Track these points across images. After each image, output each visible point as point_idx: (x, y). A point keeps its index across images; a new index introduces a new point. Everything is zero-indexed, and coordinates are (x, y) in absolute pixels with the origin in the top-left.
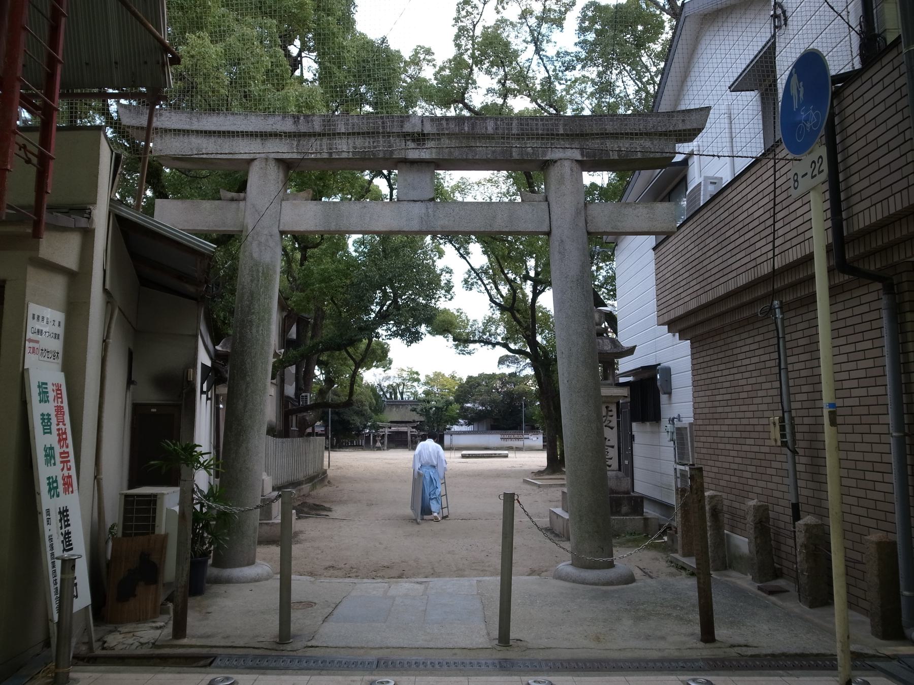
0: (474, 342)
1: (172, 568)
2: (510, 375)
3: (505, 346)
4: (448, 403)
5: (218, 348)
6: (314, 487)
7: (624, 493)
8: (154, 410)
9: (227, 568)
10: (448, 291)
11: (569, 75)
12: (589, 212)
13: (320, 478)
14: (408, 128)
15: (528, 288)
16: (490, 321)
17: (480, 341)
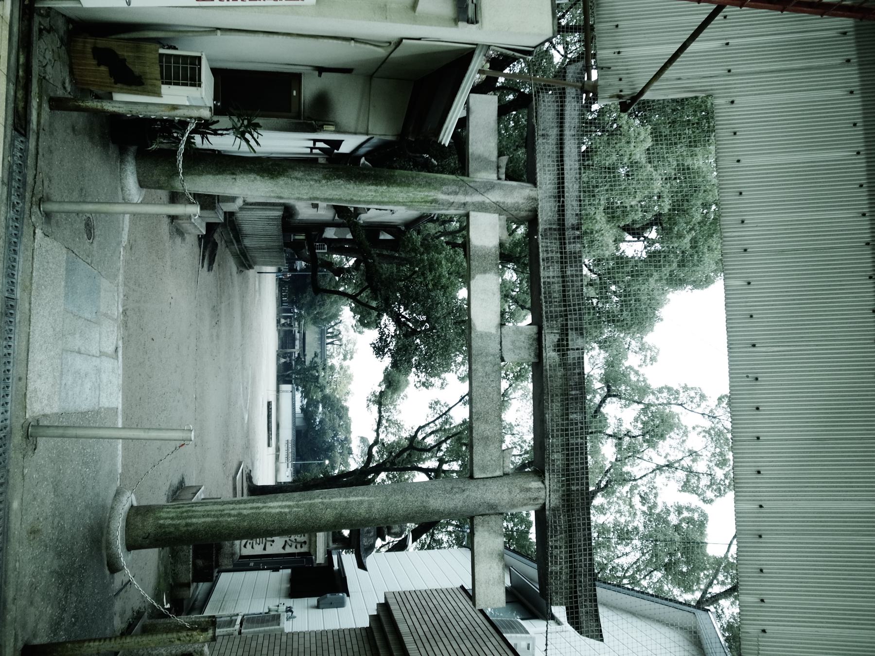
0: (380, 412)
1: (125, 101)
2: (350, 449)
3: (376, 442)
4: (322, 388)
5: (363, 160)
6: (234, 255)
8: (295, 93)
9: (136, 161)
10: (424, 384)
11: (636, 500)
13: (245, 262)
14: (572, 335)
15: (432, 464)
16: (400, 427)
17: (380, 417)
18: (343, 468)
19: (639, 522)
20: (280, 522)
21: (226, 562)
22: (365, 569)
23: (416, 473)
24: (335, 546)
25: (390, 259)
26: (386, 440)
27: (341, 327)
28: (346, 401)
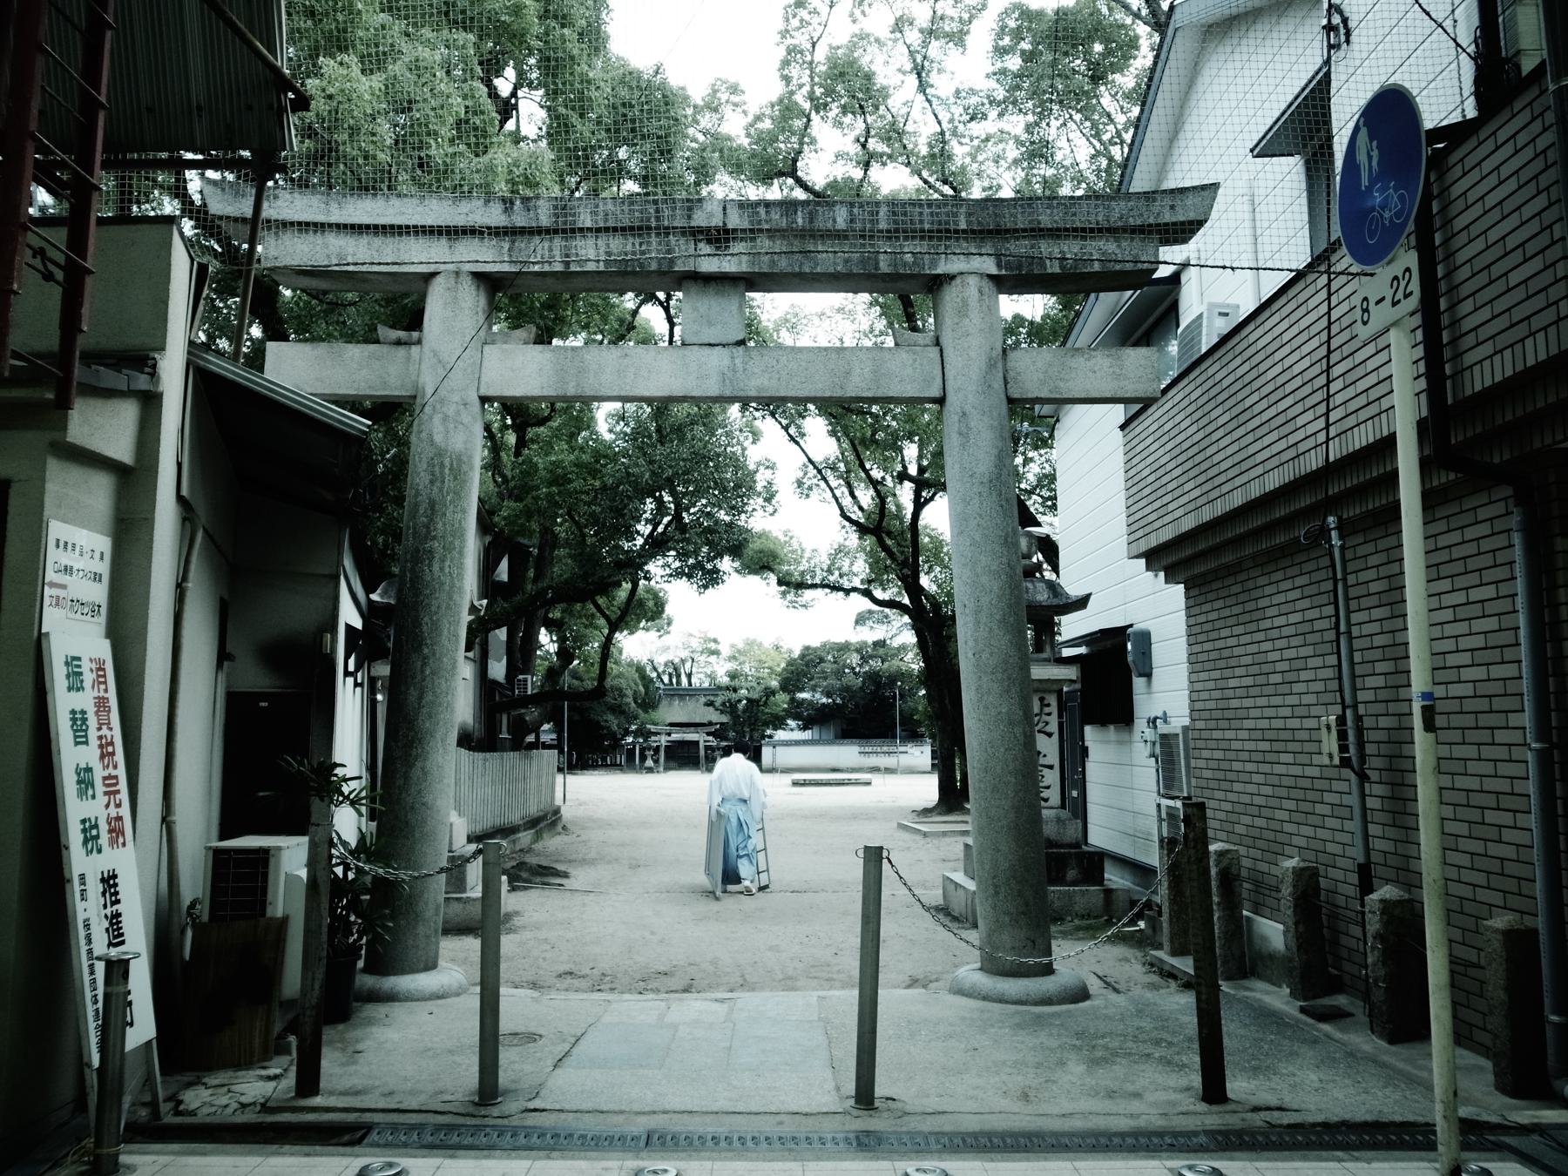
0: (814, 586)
2: (877, 644)
3: (867, 593)
4: (769, 692)
5: (375, 597)
6: (538, 837)
7: (1070, 846)
10: (768, 500)
11: (978, 129)
12: (1010, 364)
13: (548, 820)
14: (699, 219)
15: (906, 493)
16: (840, 550)
18: (910, 655)
19: (1016, 124)
20: (1011, 723)
21: (1072, 832)
22: (1088, 596)
23: (921, 523)
24: (1048, 648)
25: (542, 563)
26: (863, 576)
27: (660, 660)
28: (790, 651)
